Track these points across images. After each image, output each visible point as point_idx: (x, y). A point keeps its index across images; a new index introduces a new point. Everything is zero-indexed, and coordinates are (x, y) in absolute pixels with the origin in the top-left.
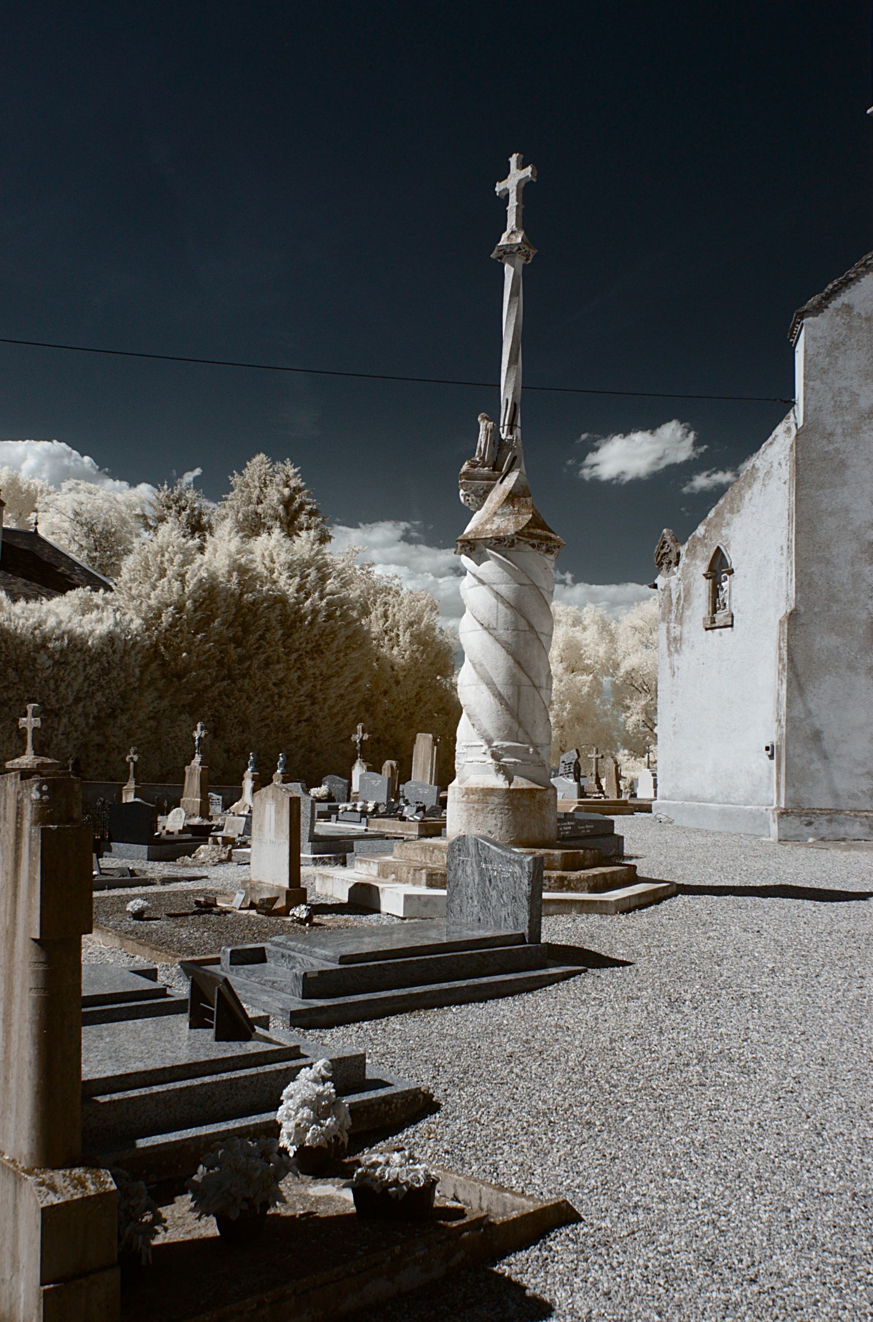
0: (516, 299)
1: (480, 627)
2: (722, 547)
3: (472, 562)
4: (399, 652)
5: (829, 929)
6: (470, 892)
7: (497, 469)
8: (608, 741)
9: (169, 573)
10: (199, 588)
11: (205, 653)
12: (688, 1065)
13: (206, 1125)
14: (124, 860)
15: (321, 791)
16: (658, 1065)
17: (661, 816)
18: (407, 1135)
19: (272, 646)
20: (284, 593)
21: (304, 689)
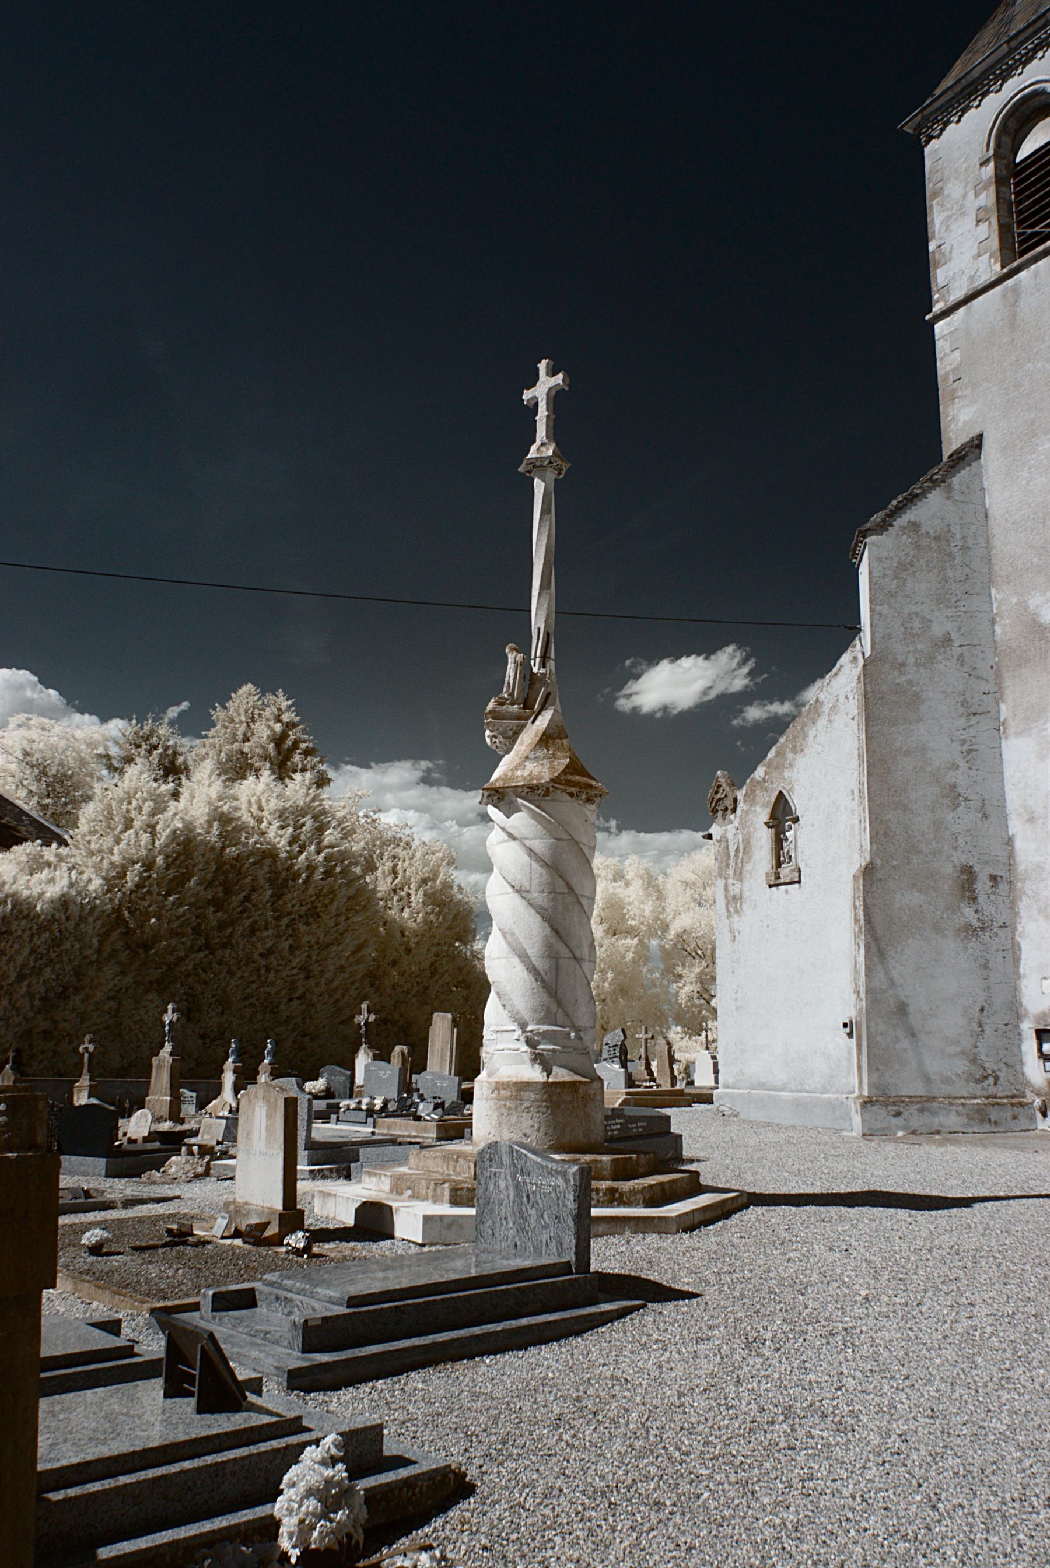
0: (547, 517)
1: (510, 890)
2: (784, 792)
3: (501, 814)
4: (411, 914)
5: (928, 1245)
6: (503, 1211)
7: (529, 707)
8: (657, 1017)
9: (137, 824)
10: (173, 840)
11: (178, 918)
12: (773, 1423)
13: (185, 1525)
14: (76, 1178)
15: (318, 1085)
16: (737, 1425)
17: (724, 1108)
18: (435, 1528)
19: (259, 909)
20: (274, 845)
21: (297, 960)
